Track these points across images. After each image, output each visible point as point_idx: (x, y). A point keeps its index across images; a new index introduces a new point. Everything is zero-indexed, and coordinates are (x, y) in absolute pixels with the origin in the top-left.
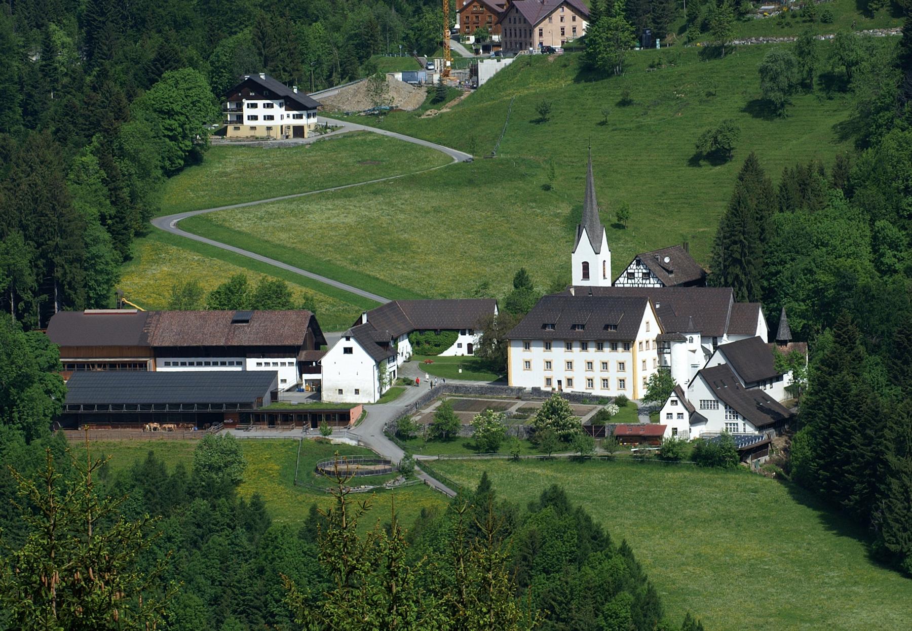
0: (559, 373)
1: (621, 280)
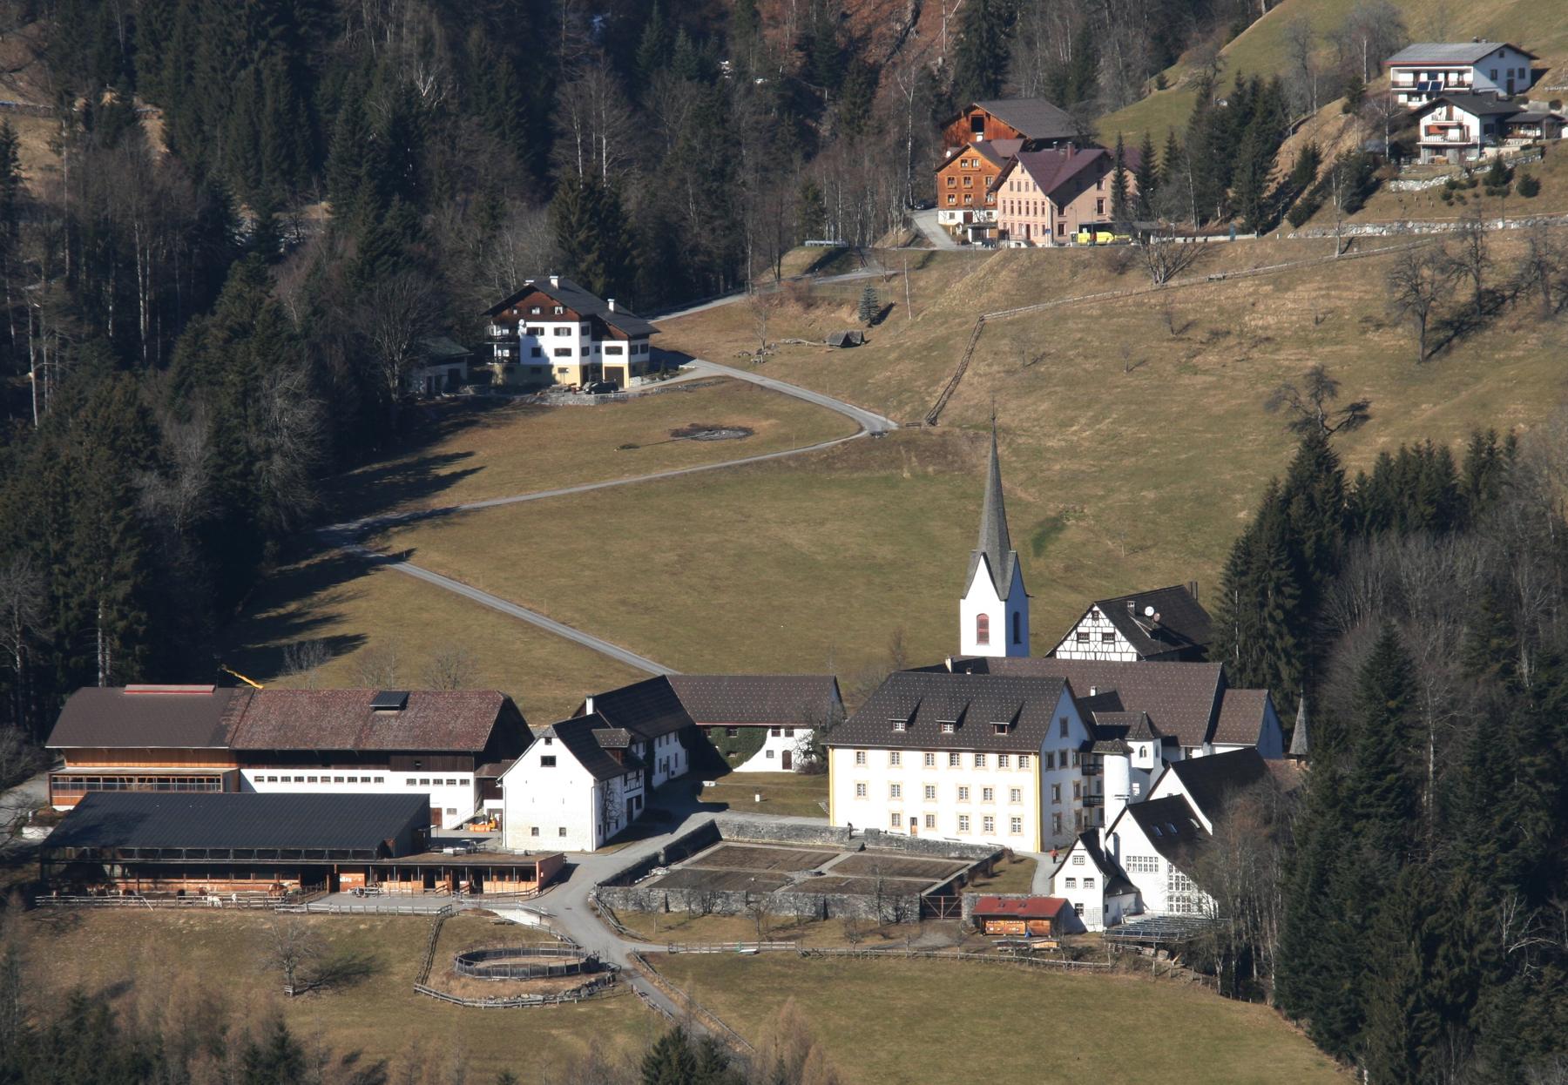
0: (913, 804)
1: (1067, 644)
